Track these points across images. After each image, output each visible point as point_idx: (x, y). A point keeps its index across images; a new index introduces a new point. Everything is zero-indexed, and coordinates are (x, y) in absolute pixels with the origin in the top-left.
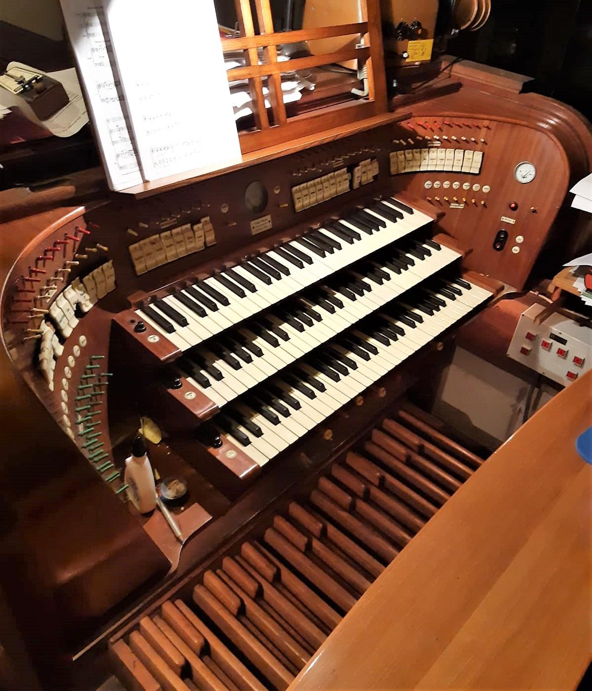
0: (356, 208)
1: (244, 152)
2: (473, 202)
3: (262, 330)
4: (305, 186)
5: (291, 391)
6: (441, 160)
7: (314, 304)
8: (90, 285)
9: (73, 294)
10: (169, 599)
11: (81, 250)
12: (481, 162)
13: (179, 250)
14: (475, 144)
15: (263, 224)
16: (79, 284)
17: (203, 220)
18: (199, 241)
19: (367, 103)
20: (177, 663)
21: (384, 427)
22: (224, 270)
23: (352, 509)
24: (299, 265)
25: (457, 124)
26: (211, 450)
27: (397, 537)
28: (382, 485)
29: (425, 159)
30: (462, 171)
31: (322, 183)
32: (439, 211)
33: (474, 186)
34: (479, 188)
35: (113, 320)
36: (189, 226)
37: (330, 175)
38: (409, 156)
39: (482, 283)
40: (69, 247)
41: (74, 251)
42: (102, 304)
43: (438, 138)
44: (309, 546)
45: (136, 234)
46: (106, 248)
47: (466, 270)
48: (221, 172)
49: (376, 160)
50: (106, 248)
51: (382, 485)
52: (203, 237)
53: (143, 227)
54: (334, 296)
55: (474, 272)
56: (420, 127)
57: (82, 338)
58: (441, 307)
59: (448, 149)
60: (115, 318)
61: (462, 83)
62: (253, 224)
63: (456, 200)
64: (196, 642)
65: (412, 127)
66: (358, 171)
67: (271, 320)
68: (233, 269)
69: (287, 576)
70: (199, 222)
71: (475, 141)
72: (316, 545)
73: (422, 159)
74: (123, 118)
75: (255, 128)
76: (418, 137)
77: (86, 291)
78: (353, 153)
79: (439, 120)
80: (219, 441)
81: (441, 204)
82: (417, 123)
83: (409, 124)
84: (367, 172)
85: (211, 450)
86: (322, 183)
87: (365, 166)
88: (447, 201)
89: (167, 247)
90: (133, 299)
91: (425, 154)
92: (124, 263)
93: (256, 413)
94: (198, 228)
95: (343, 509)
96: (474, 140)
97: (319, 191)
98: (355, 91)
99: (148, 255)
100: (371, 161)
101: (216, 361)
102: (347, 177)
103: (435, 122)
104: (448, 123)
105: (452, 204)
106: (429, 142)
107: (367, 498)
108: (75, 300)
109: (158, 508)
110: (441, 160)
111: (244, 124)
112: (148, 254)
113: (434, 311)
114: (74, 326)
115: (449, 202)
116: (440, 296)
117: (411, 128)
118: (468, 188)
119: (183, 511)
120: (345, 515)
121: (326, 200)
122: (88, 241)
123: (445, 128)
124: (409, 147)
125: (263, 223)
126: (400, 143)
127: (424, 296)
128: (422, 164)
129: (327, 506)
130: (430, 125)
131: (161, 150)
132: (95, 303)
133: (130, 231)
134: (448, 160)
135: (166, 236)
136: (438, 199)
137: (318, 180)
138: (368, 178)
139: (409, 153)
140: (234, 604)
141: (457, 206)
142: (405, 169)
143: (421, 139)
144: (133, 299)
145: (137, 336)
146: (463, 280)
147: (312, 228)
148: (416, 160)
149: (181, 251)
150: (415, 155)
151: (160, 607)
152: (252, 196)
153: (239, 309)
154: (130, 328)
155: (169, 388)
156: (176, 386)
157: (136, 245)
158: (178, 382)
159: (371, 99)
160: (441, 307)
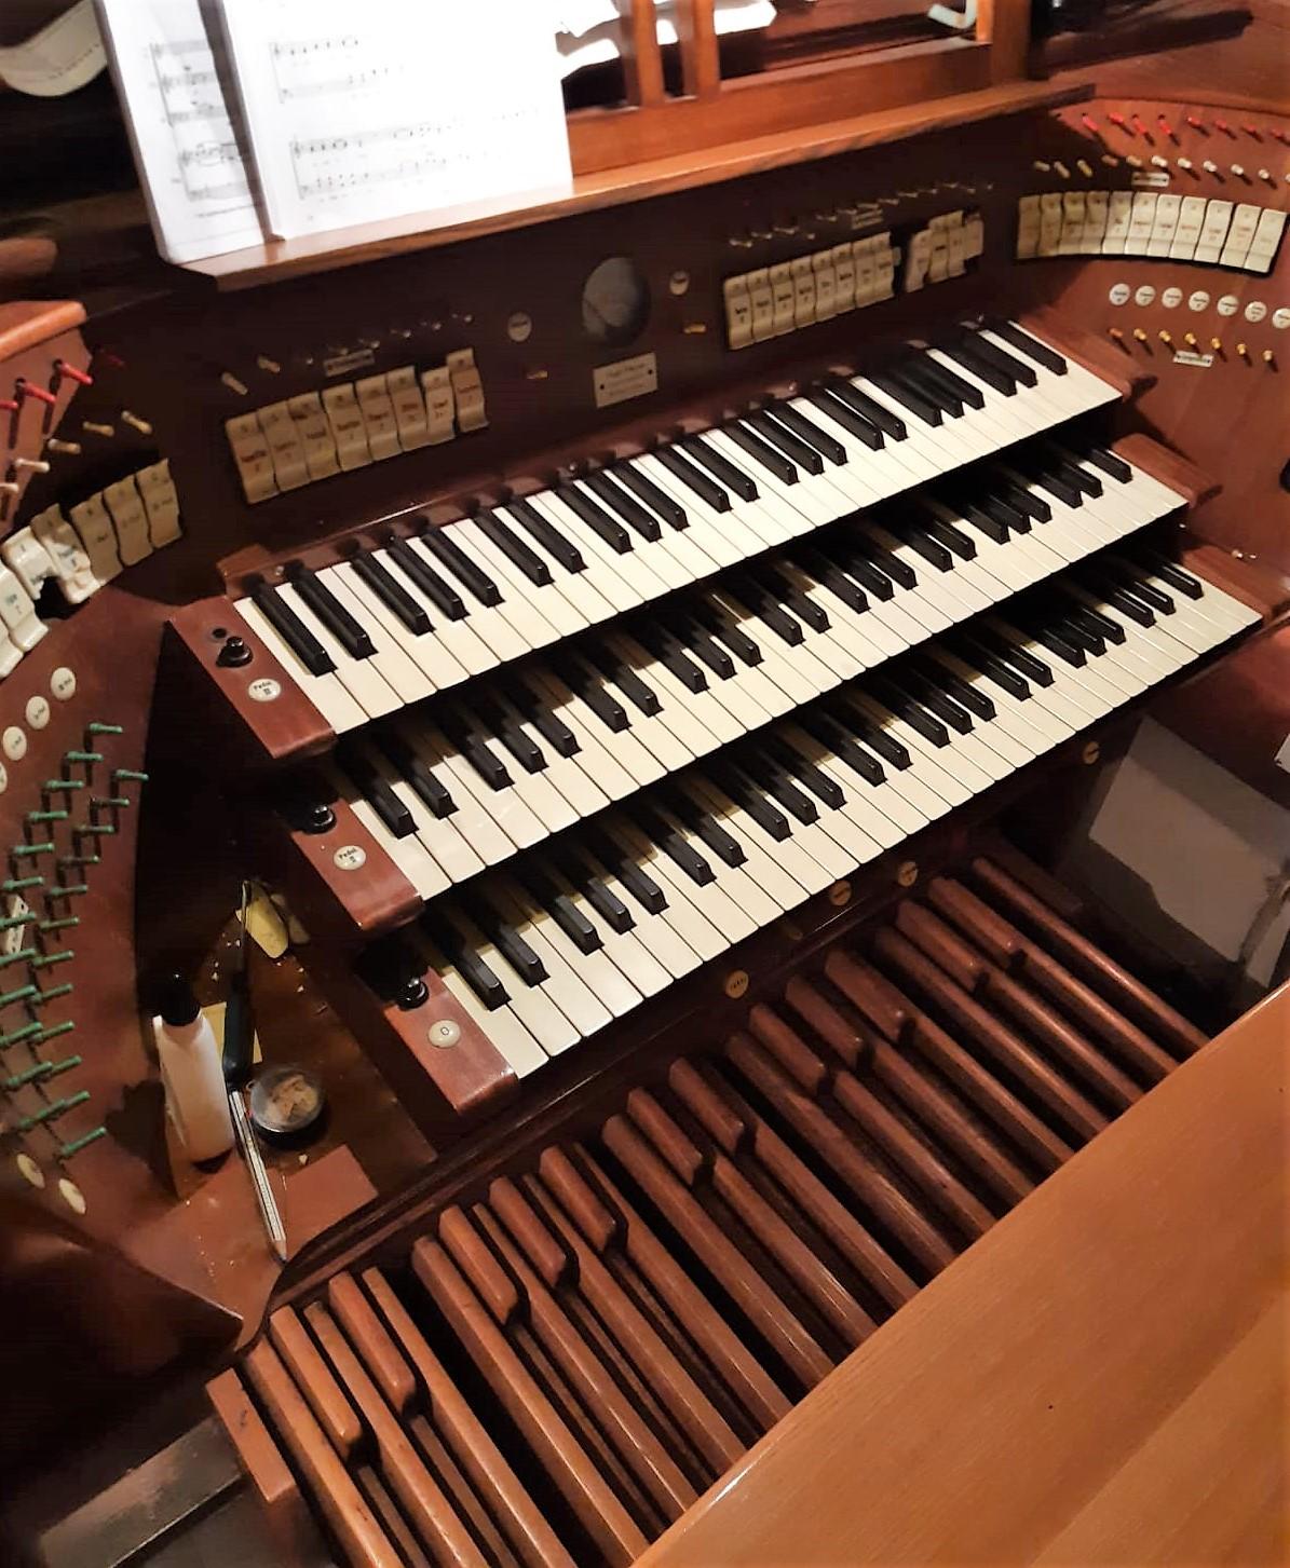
0: (905, 349)
1: (580, 170)
2: (1242, 351)
3: (589, 677)
4: (786, 273)
5: (646, 854)
6: (1164, 226)
7: (747, 612)
8: (95, 527)
9: (32, 553)
10: (348, 1268)
11: (68, 430)
12: (1278, 239)
13: (376, 439)
14: (1268, 186)
15: (624, 379)
16: (59, 525)
17: (453, 358)
18: (437, 415)
19: (970, 48)
20: (342, 1433)
21: (932, 896)
22: (506, 501)
23: (824, 1094)
24: (674, 519)
25: (1224, 126)
26: (394, 1014)
27: (923, 1175)
28: (907, 1042)
29: (1118, 221)
30: (1223, 262)
31: (791, 277)
32: (1141, 374)
33: (1251, 306)
34: (1263, 313)
35: (168, 625)
36: (408, 372)
37: (838, 250)
38: (1076, 210)
39: (1234, 583)
40: (32, 412)
41: (45, 429)
42: (127, 581)
43: (1163, 163)
44: (705, 1173)
45: (242, 390)
46: (144, 427)
47: (1193, 542)
48: (489, 226)
49: (977, 215)
50: (144, 427)
51: (907, 1042)
52: (450, 408)
53: (267, 370)
54: (808, 594)
55: (1214, 550)
56: (1117, 129)
57: (63, 679)
58: (1108, 643)
59: (1187, 198)
60: (173, 620)
61: (1255, 14)
62: (601, 375)
63: (1193, 341)
64: (395, 1384)
65: (1094, 127)
66: (921, 243)
67: (615, 649)
68: (634, 463)
69: (642, 1242)
70: (441, 363)
71: (1268, 181)
72: (724, 1171)
73: (1111, 220)
74: (206, 44)
75: (625, 102)
76: (1107, 159)
77: (82, 544)
78: (912, 191)
79: (1174, 112)
80: (417, 989)
81: (1149, 351)
82: (1108, 118)
83: (1084, 119)
84: (947, 247)
85: (394, 1014)
86: (791, 277)
87: (946, 229)
88: (1168, 344)
89: (342, 428)
90: (227, 568)
91: (1121, 207)
92: (208, 475)
93: (538, 912)
94: (437, 379)
95: (802, 1090)
96: (1265, 175)
97: (781, 299)
98: (939, 13)
99: (279, 449)
100: (965, 216)
101: (445, 758)
102: (890, 259)
103: (1162, 117)
104: (1197, 123)
105: (1180, 353)
106: (1137, 174)
107: (866, 1069)
108: (41, 570)
109: (240, 1147)
110: (1164, 226)
111: (583, 91)
112: (282, 447)
113: (1088, 655)
114: (28, 644)
115: (1171, 348)
116: (1109, 611)
117: (1089, 129)
118: (1232, 311)
119: (302, 1167)
120: (802, 1104)
121: (759, 340)
122: (84, 405)
123: (1186, 136)
124: (1078, 183)
125: (630, 374)
126: (1054, 172)
127: (1065, 611)
128: (1108, 235)
129: (769, 1079)
130: (1145, 123)
131: (323, 148)
132: (112, 576)
133: (230, 380)
134: (1184, 227)
135: (340, 398)
136: (1143, 337)
137: (805, 261)
138: (948, 264)
139: (1074, 202)
140: (501, 1296)
141: (1191, 359)
142: (1058, 243)
143: (1114, 162)
144: (227, 568)
145: (222, 677)
146: (1182, 569)
147: (773, 396)
148: (1092, 222)
149: (384, 442)
150: (1094, 207)
151: (325, 1283)
152: (607, 292)
153: (530, 618)
154: (207, 652)
155: (297, 830)
156: (318, 826)
157: (249, 419)
158: (324, 815)
159: (982, 38)
160: (1108, 643)
